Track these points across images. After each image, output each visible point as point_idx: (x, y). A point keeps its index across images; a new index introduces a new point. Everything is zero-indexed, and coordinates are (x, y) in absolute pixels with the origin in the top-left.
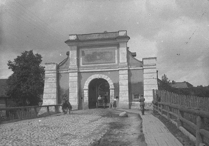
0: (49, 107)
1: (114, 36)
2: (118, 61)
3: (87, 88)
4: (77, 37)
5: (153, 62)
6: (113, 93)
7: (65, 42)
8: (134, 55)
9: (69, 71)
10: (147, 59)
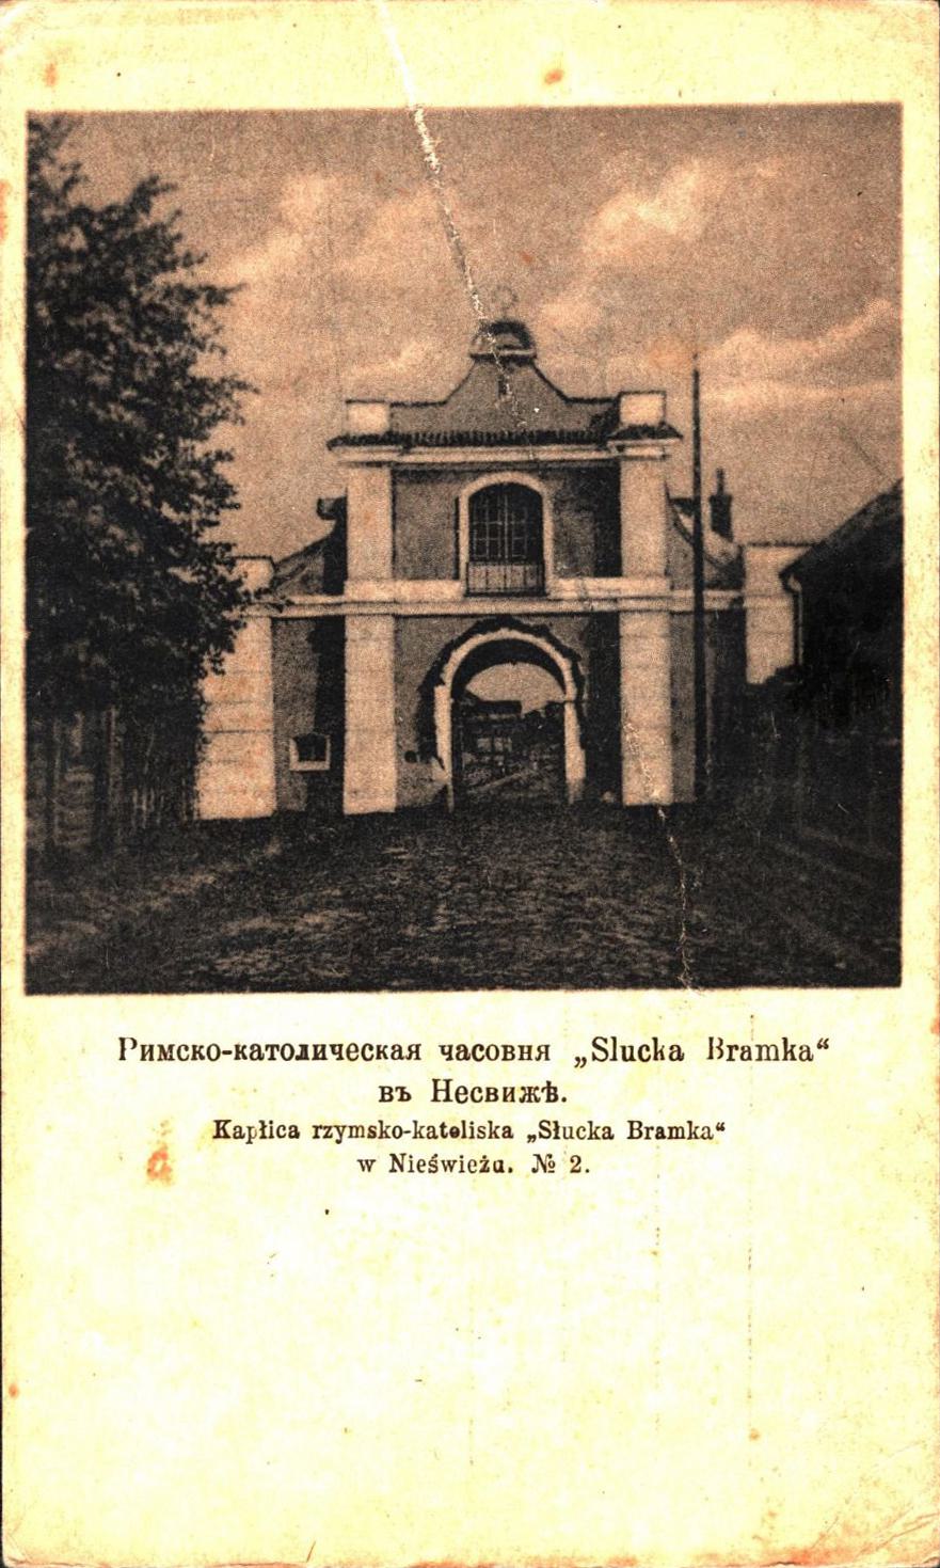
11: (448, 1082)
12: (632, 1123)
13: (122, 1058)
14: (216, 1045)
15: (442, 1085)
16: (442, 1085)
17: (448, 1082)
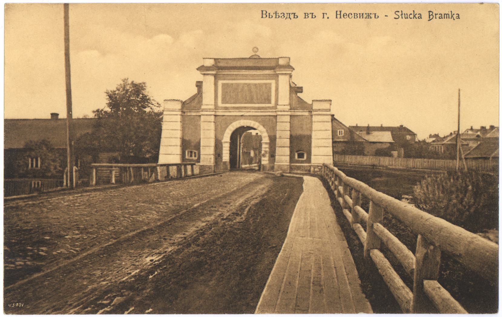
0: (170, 167)
1: (273, 64)
2: (268, 67)
3: (228, 140)
4: (216, 63)
5: (326, 106)
6: (267, 150)
7: (197, 69)
8: (300, 90)
9: (201, 113)
10: (317, 101)
11: (340, 11)
12: (305, 14)
13: (323, 18)
14: (396, 12)
15: (338, 13)
16: (338, 13)
17: (340, 11)
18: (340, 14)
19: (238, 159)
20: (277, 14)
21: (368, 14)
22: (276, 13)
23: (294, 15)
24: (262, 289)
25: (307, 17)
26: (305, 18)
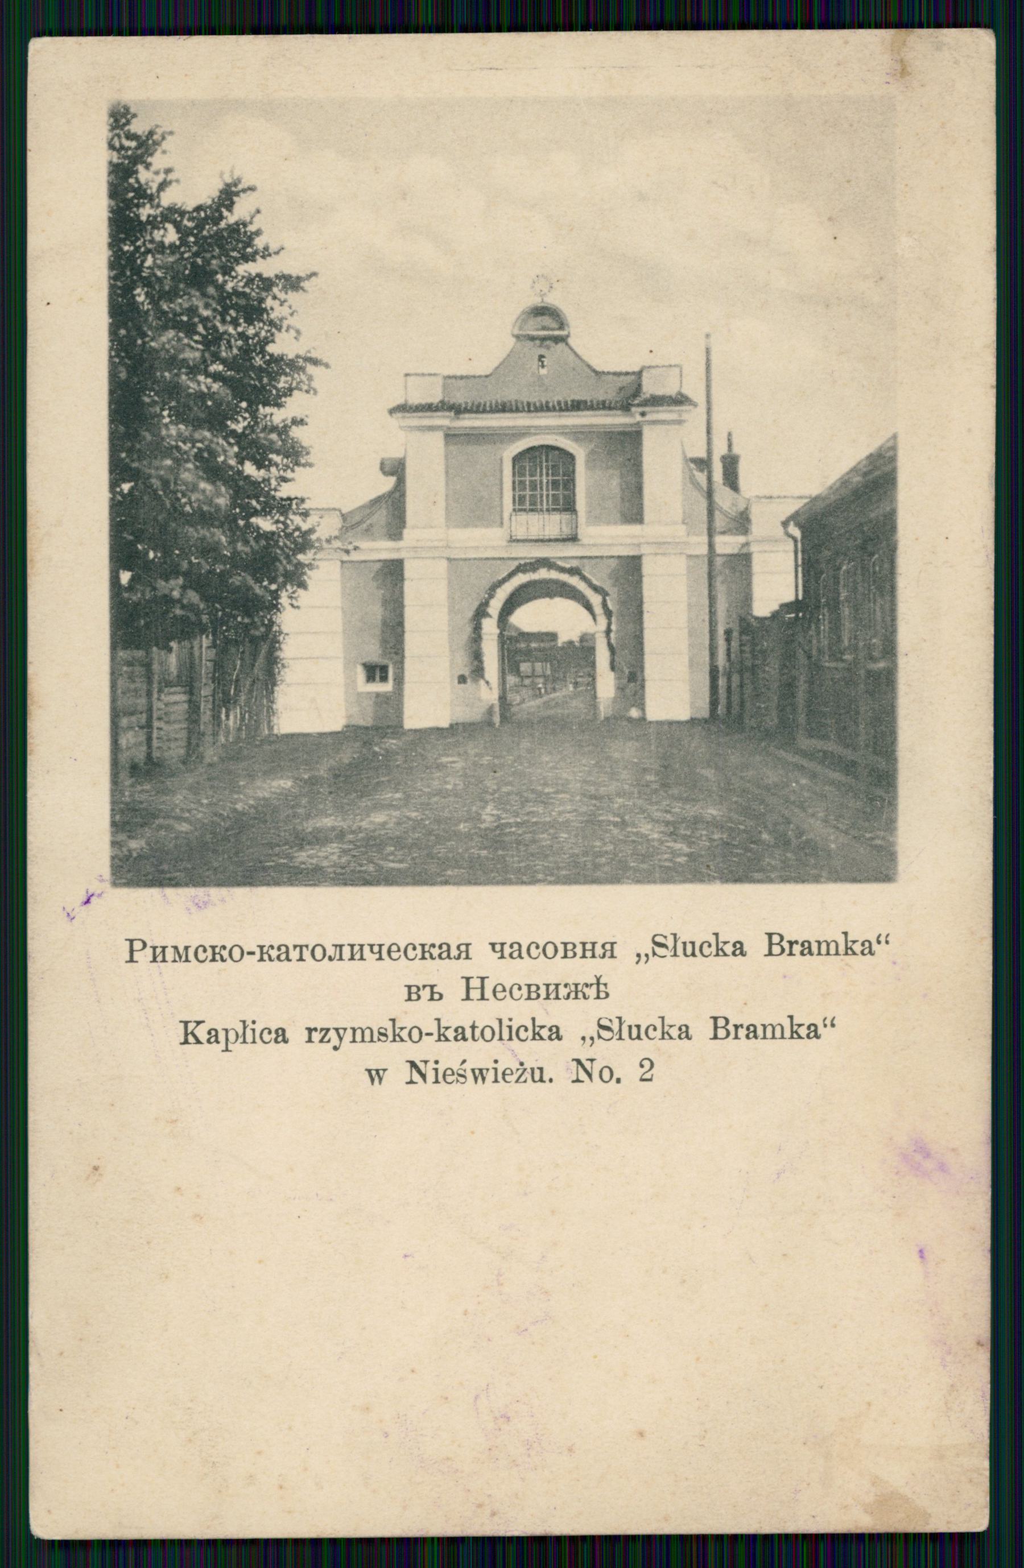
18: (482, 988)
19: (800, 575)
20: (602, 987)
21: (576, 985)
22: (598, 984)
23: (432, 993)
24: (124, 758)
25: (414, 997)
26: (409, 999)
